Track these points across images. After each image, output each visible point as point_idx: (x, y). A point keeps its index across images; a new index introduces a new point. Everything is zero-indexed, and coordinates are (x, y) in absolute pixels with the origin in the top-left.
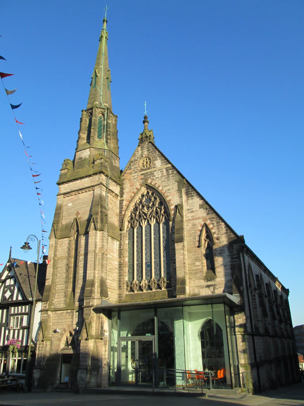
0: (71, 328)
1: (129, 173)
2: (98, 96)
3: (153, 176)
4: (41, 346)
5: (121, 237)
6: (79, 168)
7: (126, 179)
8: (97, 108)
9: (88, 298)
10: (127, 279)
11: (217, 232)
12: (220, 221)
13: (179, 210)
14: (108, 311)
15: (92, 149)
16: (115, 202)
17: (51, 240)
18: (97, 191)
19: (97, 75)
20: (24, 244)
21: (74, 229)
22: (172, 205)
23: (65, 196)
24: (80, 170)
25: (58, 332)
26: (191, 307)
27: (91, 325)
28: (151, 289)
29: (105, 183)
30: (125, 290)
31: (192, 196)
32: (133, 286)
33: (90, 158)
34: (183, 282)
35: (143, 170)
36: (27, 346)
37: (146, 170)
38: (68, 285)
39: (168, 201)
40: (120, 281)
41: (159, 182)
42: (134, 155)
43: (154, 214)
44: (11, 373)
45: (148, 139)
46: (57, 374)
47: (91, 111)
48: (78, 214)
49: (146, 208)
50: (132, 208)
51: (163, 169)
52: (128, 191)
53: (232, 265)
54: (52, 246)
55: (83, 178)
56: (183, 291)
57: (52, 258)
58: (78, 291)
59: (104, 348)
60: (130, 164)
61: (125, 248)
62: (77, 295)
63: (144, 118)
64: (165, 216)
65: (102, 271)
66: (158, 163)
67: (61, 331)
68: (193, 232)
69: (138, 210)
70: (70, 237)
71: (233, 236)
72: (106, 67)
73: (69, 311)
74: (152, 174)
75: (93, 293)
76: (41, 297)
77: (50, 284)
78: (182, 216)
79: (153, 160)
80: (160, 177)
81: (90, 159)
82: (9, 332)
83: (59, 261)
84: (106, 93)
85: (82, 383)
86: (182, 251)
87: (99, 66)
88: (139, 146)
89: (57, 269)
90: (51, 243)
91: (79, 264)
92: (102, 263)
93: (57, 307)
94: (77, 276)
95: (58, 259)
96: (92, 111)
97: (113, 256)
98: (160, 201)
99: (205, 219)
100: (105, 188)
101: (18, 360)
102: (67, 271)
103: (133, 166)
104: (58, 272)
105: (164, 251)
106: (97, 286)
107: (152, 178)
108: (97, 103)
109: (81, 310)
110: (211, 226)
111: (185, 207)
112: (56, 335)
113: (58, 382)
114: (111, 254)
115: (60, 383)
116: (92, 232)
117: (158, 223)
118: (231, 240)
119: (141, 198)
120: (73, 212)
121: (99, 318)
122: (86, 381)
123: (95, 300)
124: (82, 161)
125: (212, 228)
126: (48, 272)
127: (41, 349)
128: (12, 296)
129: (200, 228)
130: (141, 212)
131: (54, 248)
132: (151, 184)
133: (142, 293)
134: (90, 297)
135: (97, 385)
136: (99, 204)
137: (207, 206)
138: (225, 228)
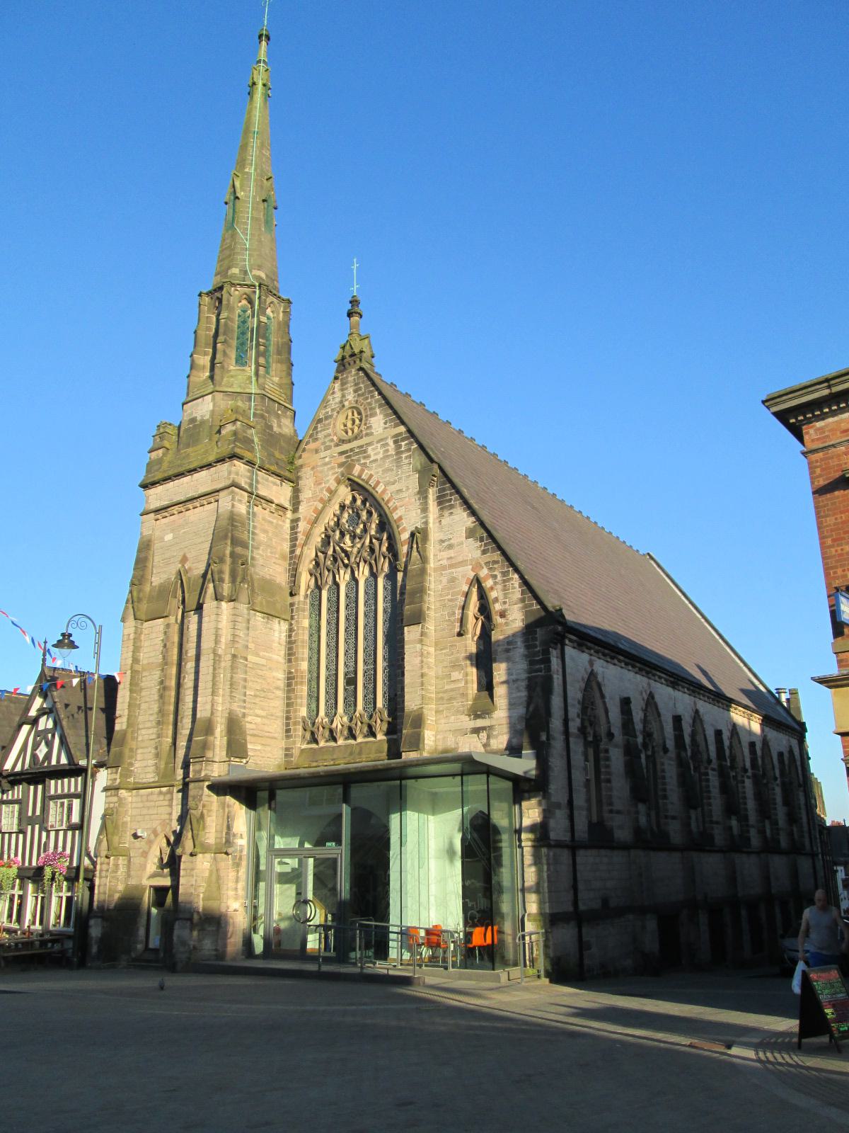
0: (168, 829)
1: (311, 451)
2: (238, 253)
3: (365, 458)
4: (105, 867)
5: (292, 611)
6: (188, 446)
7: (305, 465)
8: (233, 285)
9: (197, 760)
10: (303, 712)
11: (501, 598)
12: (511, 569)
13: (417, 543)
14: (249, 792)
15: (219, 396)
16: (277, 524)
17: (127, 624)
18: (225, 500)
19: (238, 195)
20: (61, 638)
21: (176, 597)
22: (404, 530)
23: (159, 516)
24: (190, 450)
25: (141, 837)
26: (419, 780)
27: (203, 822)
28: (354, 738)
29: (246, 483)
30: (299, 740)
31: (452, 507)
32: (316, 730)
33: (212, 418)
34: (419, 721)
35: (343, 441)
36: (78, 868)
37: (350, 441)
38: (162, 729)
39: (395, 521)
40: (288, 718)
41: (378, 473)
42: (325, 403)
43: (365, 554)
44: (54, 926)
45: (358, 362)
46: (138, 930)
47: (218, 294)
48: (184, 559)
49: (350, 539)
50: (319, 540)
51: (387, 438)
52: (310, 496)
53: (529, 679)
54: (129, 639)
55: (194, 470)
56: (417, 743)
57: (129, 667)
58: (182, 743)
59: (232, 874)
60: (316, 428)
61: (301, 637)
62: (180, 752)
63: (351, 302)
64: (389, 558)
65: (232, 697)
66: (379, 423)
67: (149, 835)
68: (450, 597)
69: (332, 544)
70: (166, 617)
71: (536, 607)
72: (262, 170)
73: (164, 789)
74: (363, 451)
75: (209, 749)
76: (106, 758)
77: (124, 727)
78: (424, 559)
79: (366, 416)
80: (381, 459)
81: (212, 421)
82: (48, 837)
83: (144, 674)
84: (260, 241)
85: (182, 949)
86: (419, 646)
87: (244, 168)
88: (336, 378)
89: (141, 692)
90: (126, 632)
91: (186, 681)
92: (232, 677)
93: (140, 781)
94: (180, 709)
95: (144, 670)
96: (222, 295)
97: (269, 659)
98: (379, 522)
99: (477, 567)
100: (246, 494)
101: (67, 897)
102: (161, 696)
103: (321, 431)
104: (143, 700)
105: (385, 644)
106: (221, 731)
107: (362, 461)
108: (235, 271)
109: (185, 789)
110: (488, 584)
111: (434, 535)
112: (137, 843)
113: (140, 947)
114: (262, 654)
115: (147, 948)
116: (209, 605)
117: (374, 575)
118: (531, 619)
119: (338, 512)
120: (174, 556)
121: (223, 805)
122: (189, 945)
123: (216, 765)
124: (195, 426)
125: (492, 588)
126: (119, 700)
127: (104, 874)
128: (48, 756)
129: (466, 588)
130: (337, 548)
131: (131, 642)
132: (359, 477)
133: (334, 747)
134: (201, 759)
135: (216, 955)
136: (231, 539)
137: (483, 531)
138: (520, 587)
